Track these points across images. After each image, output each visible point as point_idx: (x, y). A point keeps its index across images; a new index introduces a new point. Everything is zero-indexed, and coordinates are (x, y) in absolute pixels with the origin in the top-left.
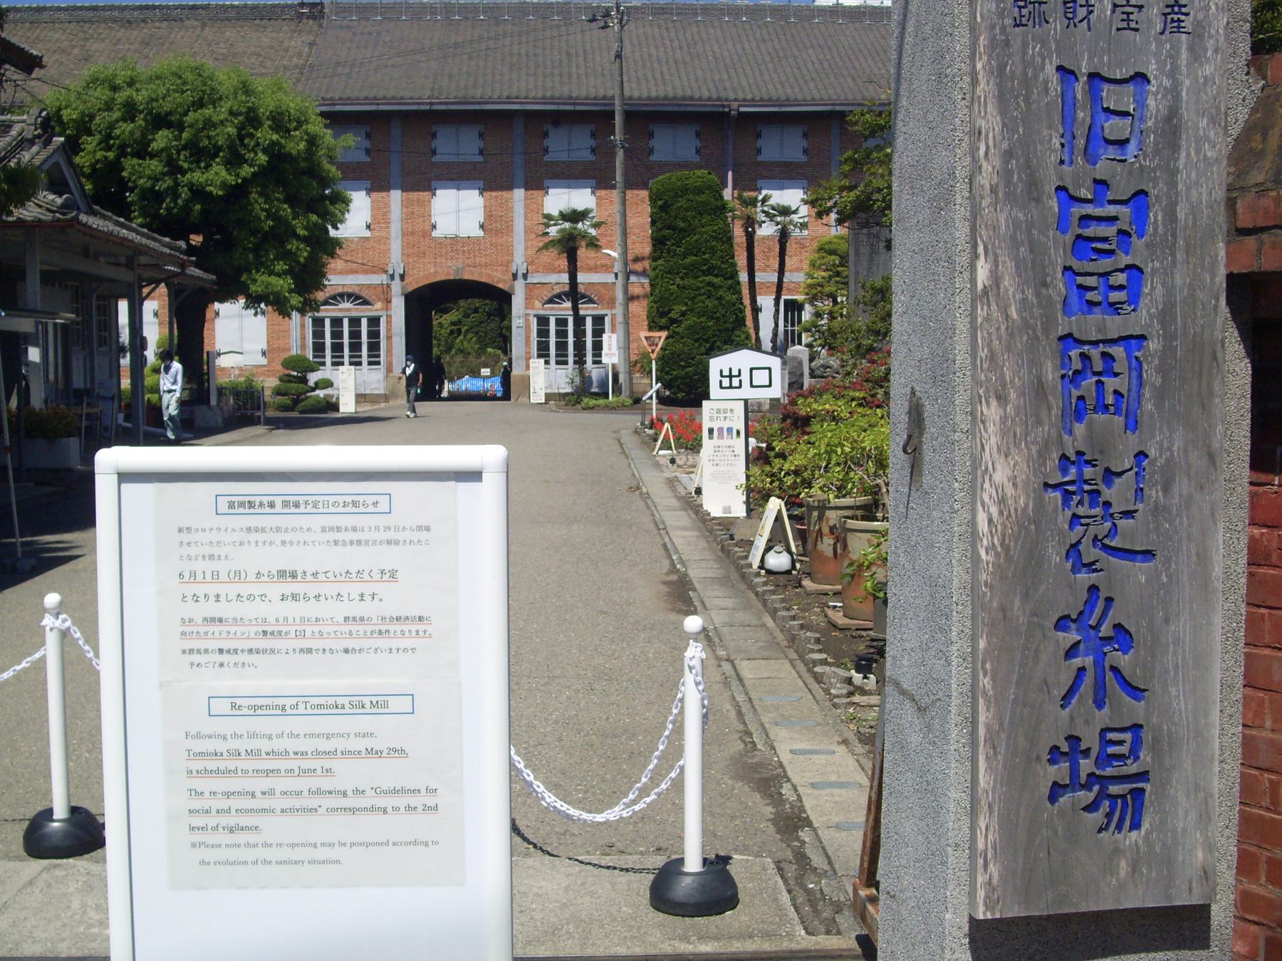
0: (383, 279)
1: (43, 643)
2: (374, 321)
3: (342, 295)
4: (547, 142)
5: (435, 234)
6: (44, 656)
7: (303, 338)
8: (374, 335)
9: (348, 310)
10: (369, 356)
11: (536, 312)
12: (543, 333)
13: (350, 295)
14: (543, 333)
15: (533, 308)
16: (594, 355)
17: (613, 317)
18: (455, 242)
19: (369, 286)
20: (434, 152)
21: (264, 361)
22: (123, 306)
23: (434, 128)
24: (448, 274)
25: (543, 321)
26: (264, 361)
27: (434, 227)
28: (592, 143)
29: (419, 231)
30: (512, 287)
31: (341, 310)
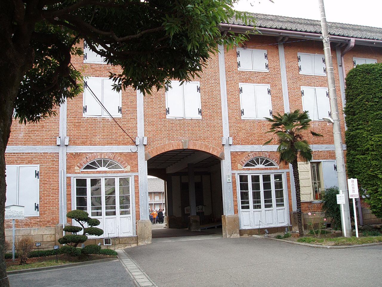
0: (133, 148)
1: (88, 165)
2: (124, 182)
3: (100, 162)
4: (239, 59)
5: (168, 116)
6: (89, 164)
7: (69, 195)
8: (244, 196)
9: (105, 172)
10: (265, 201)
11: (239, 172)
12: (244, 187)
13: (105, 162)
14: (244, 187)
15: (237, 169)
16: (254, 202)
17: (288, 174)
18: (182, 123)
19: (121, 154)
20: (300, 69)
21: (36, 214)
22: (279, 179)
23: (299, 54)
24: (179, 145)
25: (243, 179)
26: (36, 214)
27: (168, 111)
28: (266, 61)
29: (158, 116)
30: (223, 154)
31: (99, 172)
